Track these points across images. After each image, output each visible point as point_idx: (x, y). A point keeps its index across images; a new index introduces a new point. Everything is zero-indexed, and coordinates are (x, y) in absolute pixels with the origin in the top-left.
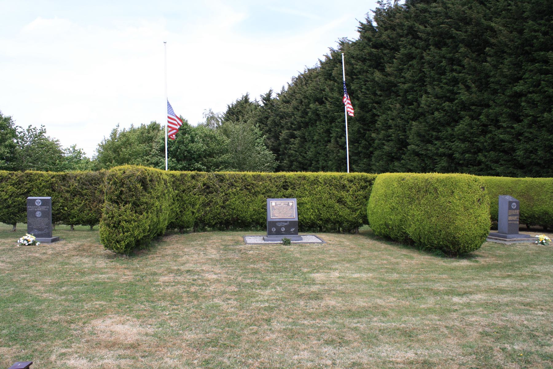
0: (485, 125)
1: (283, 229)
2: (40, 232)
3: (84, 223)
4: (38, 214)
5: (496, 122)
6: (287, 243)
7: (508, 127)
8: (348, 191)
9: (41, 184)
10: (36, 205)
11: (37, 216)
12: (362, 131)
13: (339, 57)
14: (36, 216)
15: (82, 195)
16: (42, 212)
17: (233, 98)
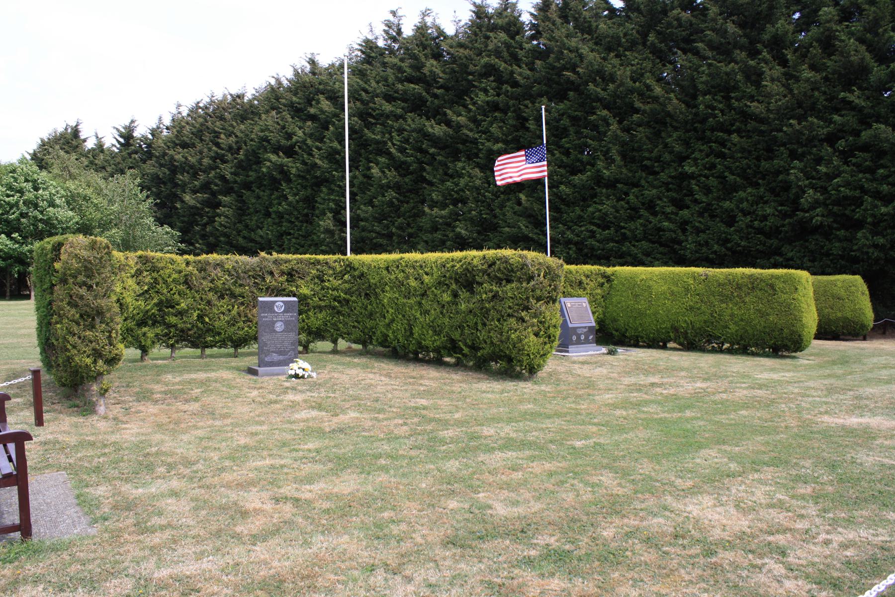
0: (635, 209)
1: (583, 337)
2: (281, 358)
3: (223, 344)
4: (279, 327)
5: (650, 206)
6: (611, 353)
7: (672, 213)
8: (585, 289)
9: (169, 276)
10: (274, 312)
11: (278, 329)
12: (396, 202)
13: (337, 86)
14: (275, 331)
15: (233, 295)
16: (286, 323)
17: (55, 124)
